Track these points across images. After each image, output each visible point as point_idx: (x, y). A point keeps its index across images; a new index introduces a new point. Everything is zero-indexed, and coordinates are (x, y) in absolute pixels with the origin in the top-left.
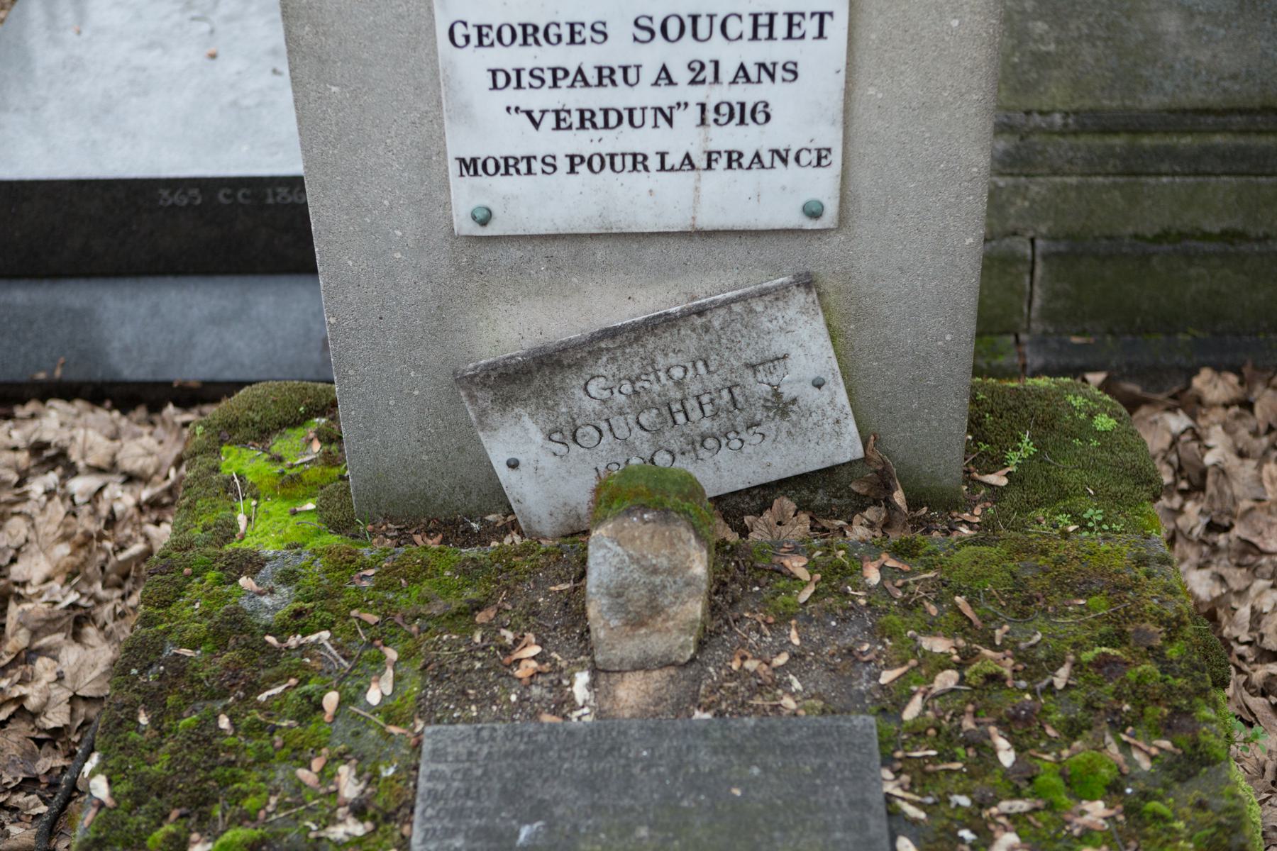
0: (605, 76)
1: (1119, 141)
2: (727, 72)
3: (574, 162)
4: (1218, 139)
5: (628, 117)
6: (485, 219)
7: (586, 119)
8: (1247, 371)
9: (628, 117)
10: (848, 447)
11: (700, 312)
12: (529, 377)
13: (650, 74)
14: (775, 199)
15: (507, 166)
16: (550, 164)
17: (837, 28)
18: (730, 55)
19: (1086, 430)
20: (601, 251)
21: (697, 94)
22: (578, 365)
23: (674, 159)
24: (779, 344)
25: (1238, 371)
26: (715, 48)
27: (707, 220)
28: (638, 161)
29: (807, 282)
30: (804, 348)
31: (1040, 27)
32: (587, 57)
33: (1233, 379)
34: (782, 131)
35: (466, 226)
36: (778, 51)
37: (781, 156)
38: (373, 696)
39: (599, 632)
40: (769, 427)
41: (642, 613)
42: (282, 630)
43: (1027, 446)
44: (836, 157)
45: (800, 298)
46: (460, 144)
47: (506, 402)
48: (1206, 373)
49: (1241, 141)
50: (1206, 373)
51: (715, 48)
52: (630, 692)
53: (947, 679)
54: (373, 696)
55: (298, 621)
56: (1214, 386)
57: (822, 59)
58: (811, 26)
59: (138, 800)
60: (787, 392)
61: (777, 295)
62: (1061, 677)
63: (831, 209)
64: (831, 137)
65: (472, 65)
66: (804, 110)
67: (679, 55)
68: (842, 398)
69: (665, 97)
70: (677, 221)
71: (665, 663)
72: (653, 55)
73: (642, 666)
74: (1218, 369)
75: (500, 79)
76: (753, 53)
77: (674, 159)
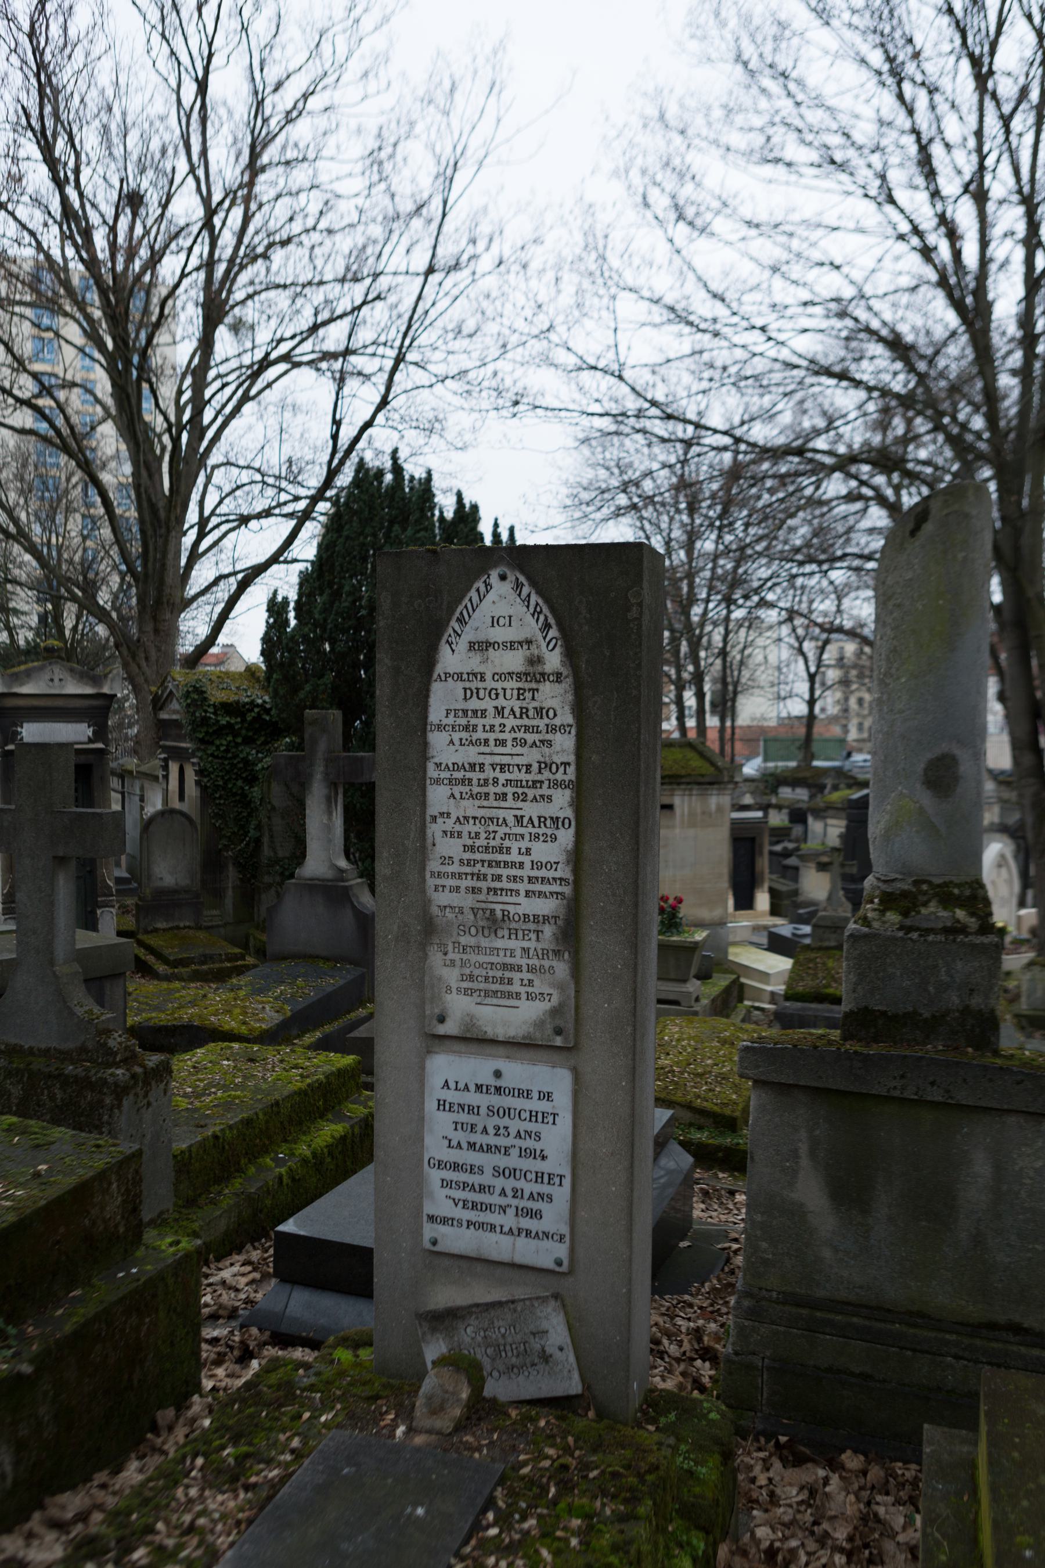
0: (482, 1189)
1: (805, 1312)
2: (526, 1195)
3: (469, 1223)
4: (855, 1320)
5: (489, 1208)
6: (434, 1243)
7: (474, 1206)
8: (871, 1456)
9: (489, 1208)
10: (575, 1387)
11: (513, 1302)
12: (444, 1319)
13: (498, 1191)
14: (546, 1254)
15: (445, 1221)
16: (460, 1223)
17: (567, 1182)
18: (529, 1188)
19: (705, 1416)
20: (479, 1268)
21: (515, 1202)
22: (463, 1318)
23: (506, 1229)
24: (545, 1325)
25: (866, 1455)
26: (521, 1184)
27: (519, 1259)
28: (492, 1228)
29: (556, 1296)
30: (556, 1332)
31: (764, 1245)
32: (475, 1179)
33: (862, 1458)
34: (546, 1224)
35: (427, 1245)
36: (545, 1189)
37: (546, 1235)
38: (323, 1419)
39: (418, 1413)
40: (541, 1367)
41: (436, 1409)
42: (303, 1390)
43: (672, 1416)
44: (567, 1239)
45: (552, 1303)
46: (429, 1209)
47: (434, 1330)
48: (849, 1452)
49: (867, 1323)
50: (849, 1452)
51: (521, 1184)
52: (419, 1440)
53: (546, 1463)
54: (323, 1419)
55: (312, 1388)
56: (852, 1461)
57: (562, 1194)
58: (557, 1180)
59: (217, 1430)
60: (549, 1350)
61: (544, 1300)
62: (593, 1474)
63: (566, 1263)
64: (565, 1230)
65: (435, 1176)
66: (554, 1216)
67: (509, 1184)
68: (572, 1358)
69: (503, 1201)
70: (505, 1257)
71: (439, 1433)
72: (499, 1183)
73: (429, 1432)
74: (856, 1451)
75: (446, 1184)
76: (537, 1188)
77: (506, 1229)
